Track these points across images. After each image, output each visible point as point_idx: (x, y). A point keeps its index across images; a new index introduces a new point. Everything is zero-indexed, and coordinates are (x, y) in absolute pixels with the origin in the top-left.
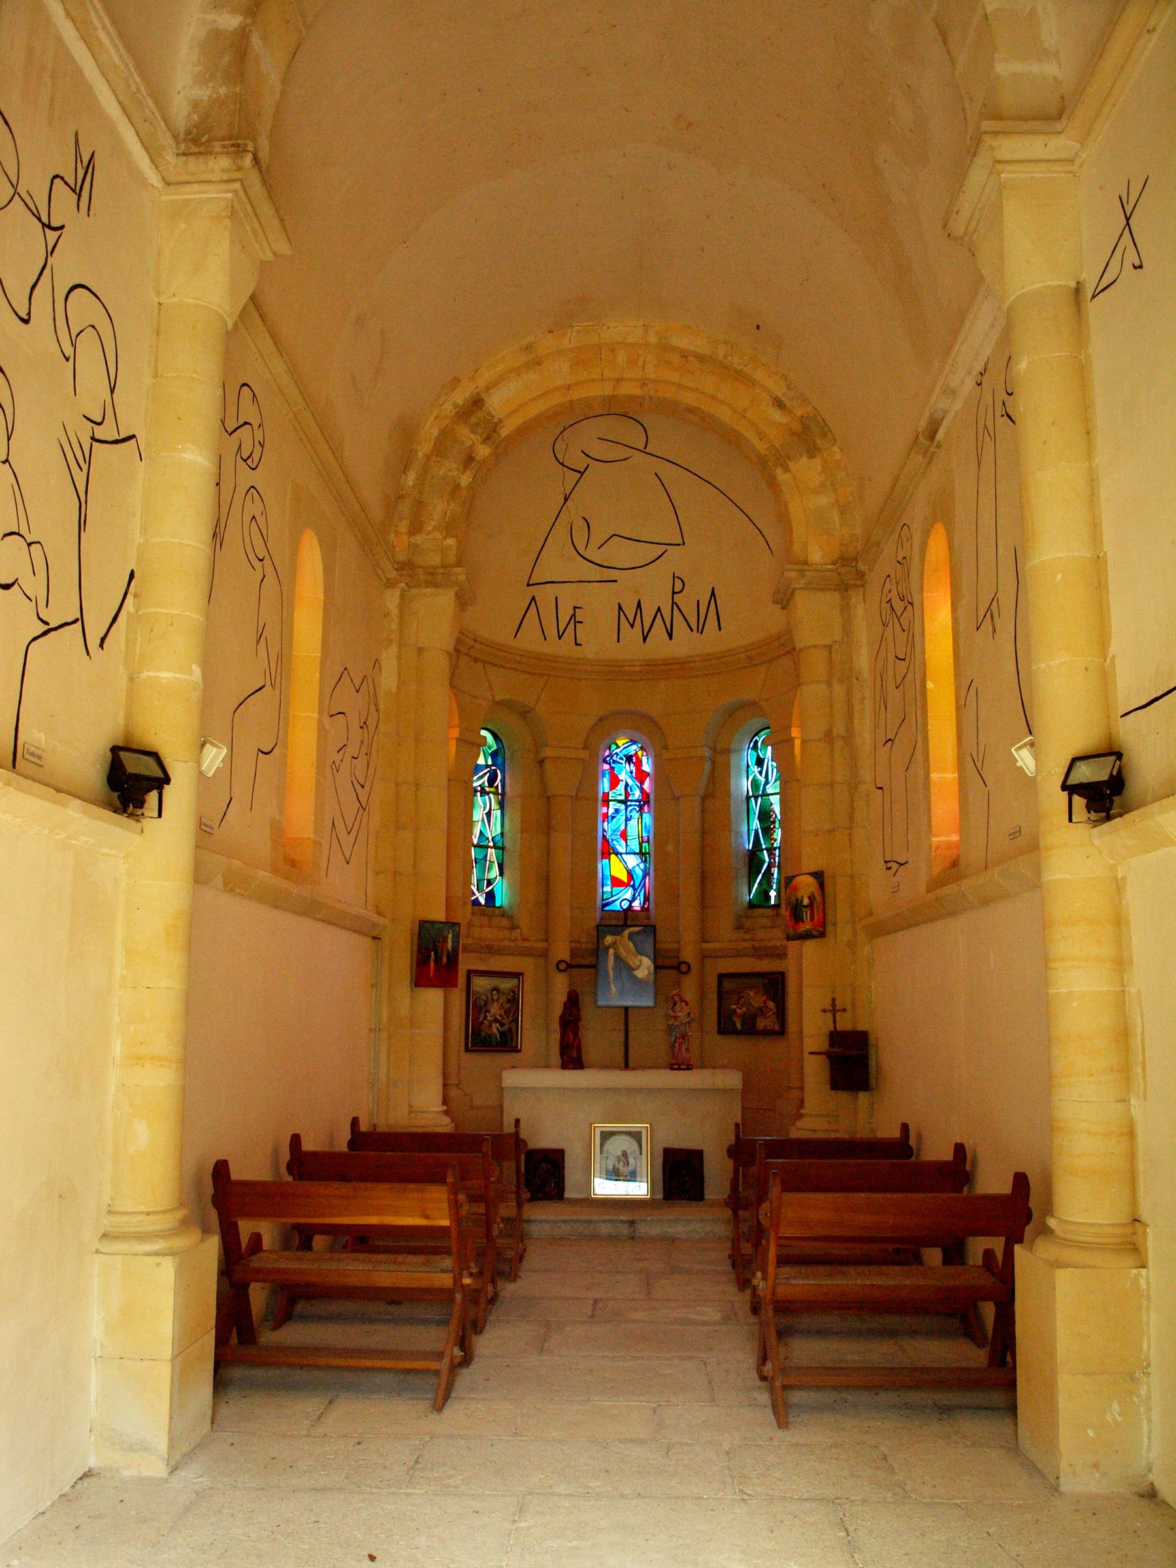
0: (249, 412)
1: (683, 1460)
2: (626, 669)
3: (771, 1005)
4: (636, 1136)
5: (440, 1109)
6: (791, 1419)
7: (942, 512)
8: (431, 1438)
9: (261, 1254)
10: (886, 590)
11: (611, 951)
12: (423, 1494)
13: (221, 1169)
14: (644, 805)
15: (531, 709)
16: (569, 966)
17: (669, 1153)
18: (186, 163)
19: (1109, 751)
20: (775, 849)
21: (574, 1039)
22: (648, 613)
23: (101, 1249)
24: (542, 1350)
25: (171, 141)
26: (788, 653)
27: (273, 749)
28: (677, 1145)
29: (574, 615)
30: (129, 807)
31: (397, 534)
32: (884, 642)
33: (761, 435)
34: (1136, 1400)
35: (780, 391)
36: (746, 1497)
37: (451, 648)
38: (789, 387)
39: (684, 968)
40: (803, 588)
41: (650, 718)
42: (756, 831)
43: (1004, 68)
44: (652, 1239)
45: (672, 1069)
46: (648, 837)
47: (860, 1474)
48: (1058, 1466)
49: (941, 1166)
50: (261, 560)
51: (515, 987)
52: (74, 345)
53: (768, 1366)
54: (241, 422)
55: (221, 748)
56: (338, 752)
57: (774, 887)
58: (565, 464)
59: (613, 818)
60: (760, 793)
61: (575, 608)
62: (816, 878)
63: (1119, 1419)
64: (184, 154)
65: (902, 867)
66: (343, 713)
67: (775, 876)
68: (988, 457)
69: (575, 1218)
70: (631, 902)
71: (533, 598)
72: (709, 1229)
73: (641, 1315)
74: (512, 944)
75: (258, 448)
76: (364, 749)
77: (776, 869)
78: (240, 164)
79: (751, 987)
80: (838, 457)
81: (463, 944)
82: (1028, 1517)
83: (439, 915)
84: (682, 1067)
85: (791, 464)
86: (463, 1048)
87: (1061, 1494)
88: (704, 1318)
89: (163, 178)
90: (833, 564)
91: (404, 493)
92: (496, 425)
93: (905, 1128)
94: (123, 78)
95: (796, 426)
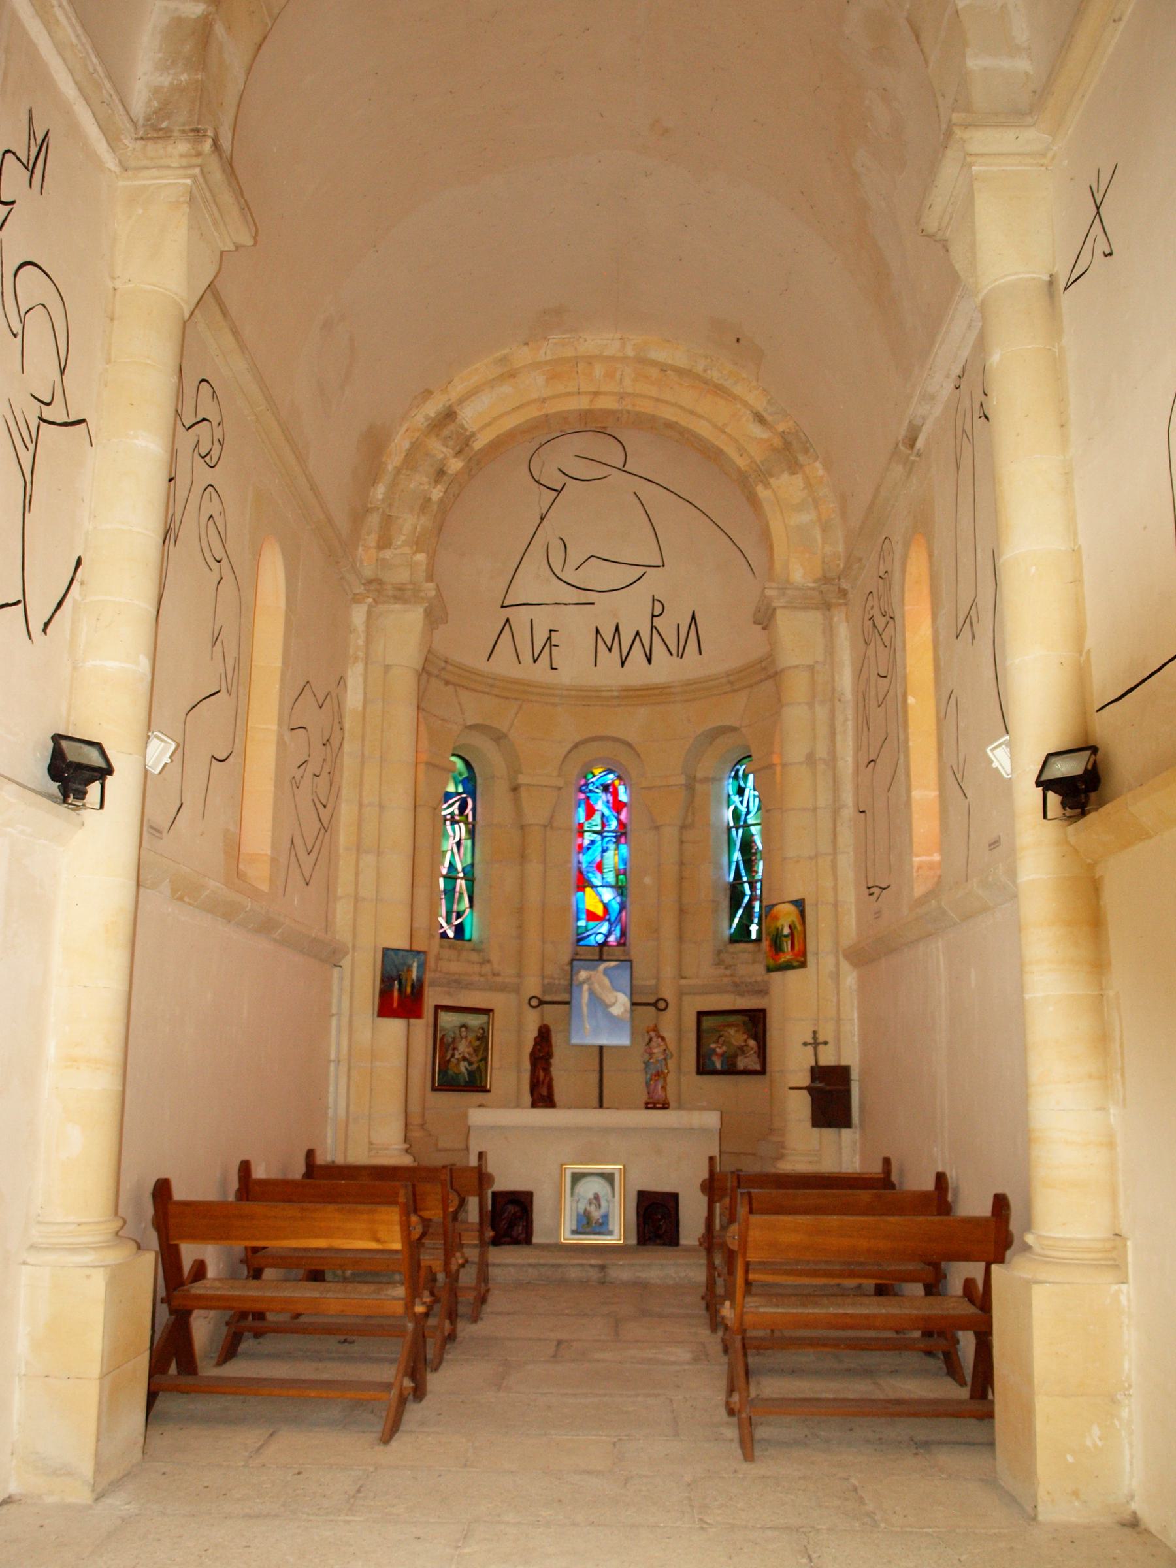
0: (207, 408)
1: (640, 1490)
2: (604, 694)
3: (752, 1043)
6: (756, 1453)
7: (922, 525)
8: (376, 1468)
10: (868, 608)
11: (586, 987)
16: (542, 1003)
17: (642, 1195)
20: (757, 881)
21: (545, 1076)
22: (627, 637)
23: (28, 1260)
24: (499, 1388)
25: (129, 125)
26: (769, 677)
27: (228, 757)
29: (549, 638)
32: (866, 660)
34: (1117, 1423)
35: (760, 405)
36: (705, 1526)
37: (419, 667)
39: (662, 1005)
41: (630, 746)
42: (737, 863)
43: (975, 63)
45: (647, 1108)
47: (827, 1504)
49: (924, 1195)
50: (219, 561)
52: (23, 323)
53: (736, 1398)
54: (200, 418)
56: (299, 767)
57: (756, 920)
59: (588, 849)
60: (742, 823)
62: (796, 906)
63: (1100, 1444)
64: (142, 138)
66: (305, 728)
68: (966, 462)
69: (542, 1261)
70: (607, 936)
71: (508, 620)
74: (482, 979)
75: (217, 446)
76: (327, 769)
78: (199, 149)
79: (730, 1025)
83: (399, 941)
84: (658, 1106)
85: (772, 480)
88: (673, 1358)
89: (120, 161)
90: (814, 582)
91: (373, 506)
93: (887, 1162)
94: (81, 58)
95: (777, 442)
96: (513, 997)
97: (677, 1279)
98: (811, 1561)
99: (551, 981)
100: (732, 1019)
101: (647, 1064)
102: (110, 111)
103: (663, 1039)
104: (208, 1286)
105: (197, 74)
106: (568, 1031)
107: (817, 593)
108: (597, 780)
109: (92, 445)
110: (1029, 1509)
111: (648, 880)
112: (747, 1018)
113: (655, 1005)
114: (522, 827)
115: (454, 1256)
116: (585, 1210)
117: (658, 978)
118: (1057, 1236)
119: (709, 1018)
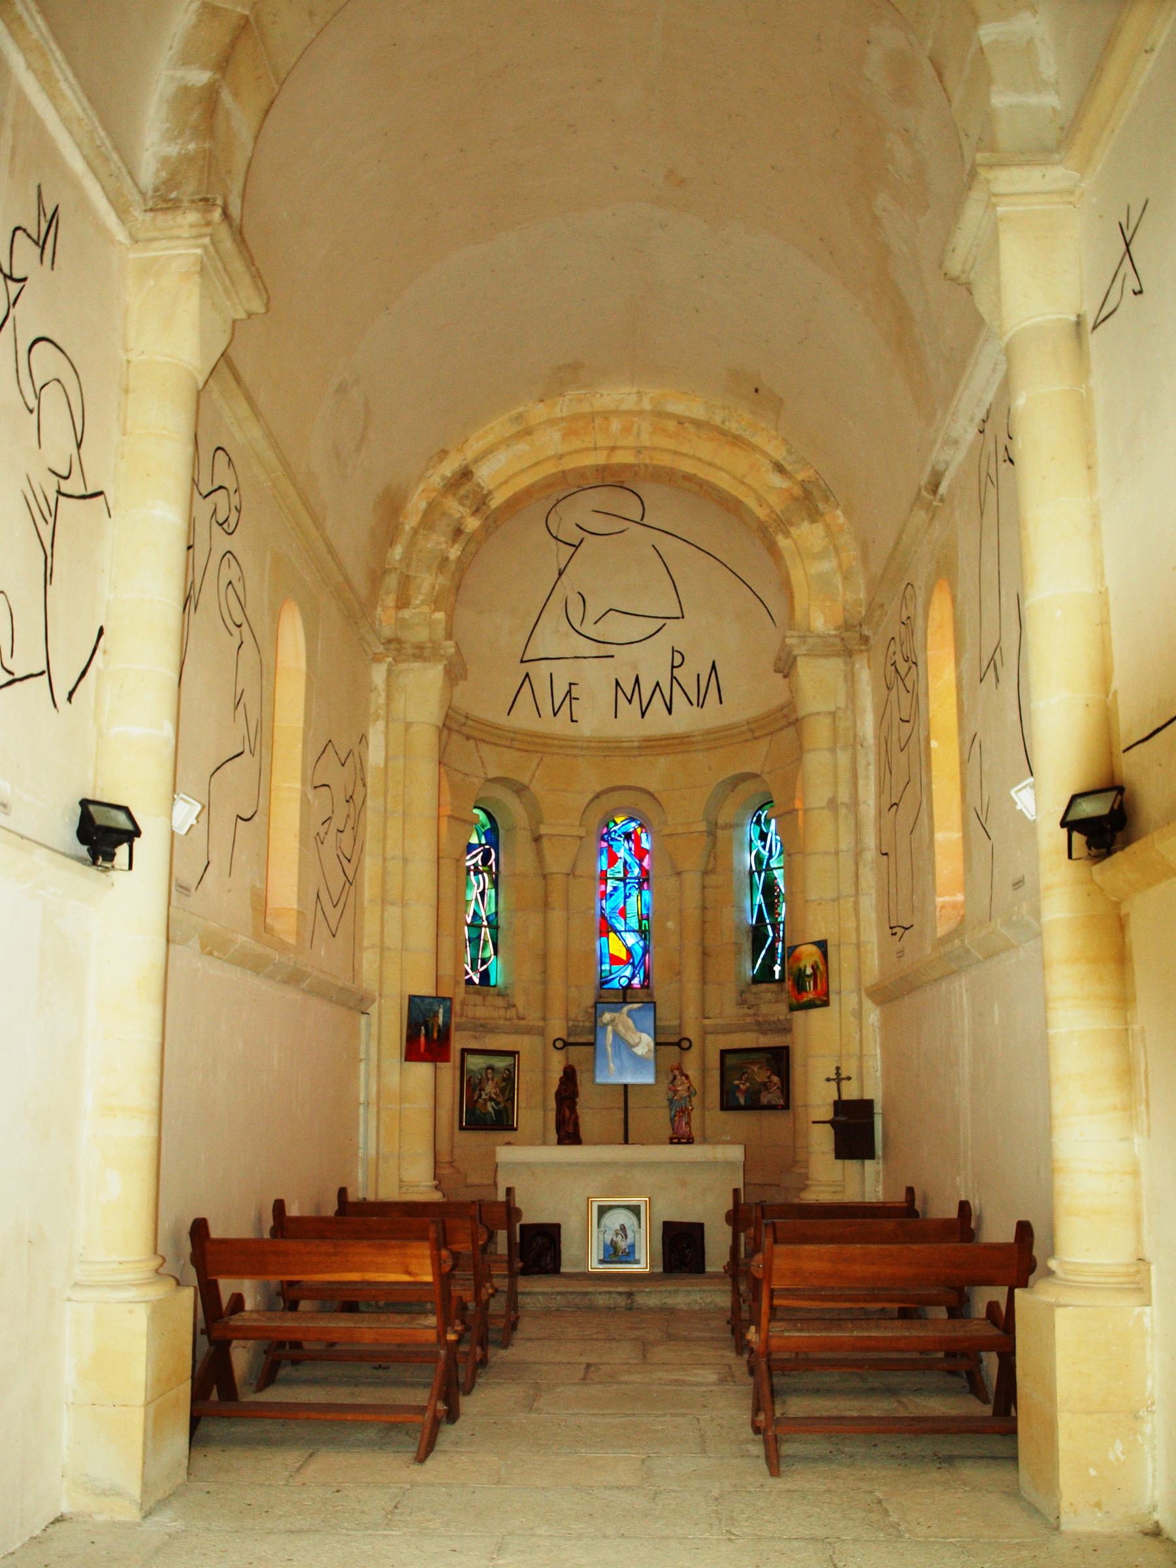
0: (224, 476)
2: (625, 744)
3: (775, 1079)
4: (635, 1210)
5: (430, 1184)
6: (783, 1468)
7: (945, 569)
8: (412, 1486)
9: (243, 1314)
11: (610, 1028)
12: (400, 1535)
13: (199, 1228)
14: (643, 882)
15: (525, 786)
16: (566, 1044)
17: (668, 1226)
18: (153, 220)
19: (1110, 786)
21: (571, 1114)
22: (646, 689)
25: (138, 197)
26: (790, 724)
27: (253, 816)
28: (677, 1218)
29: (569, 692)
30: (98, 859)
31: (385, 608)
33: (761, 501)
35: (779, 454)
36: (733, 1537)
38: (789, 452)
39: (685, 1044)
40: (805, 655)
42: (760, 906)
44: (651, 1310)
45: (672, 1143)
46: (648, 914)
48: (1059, 1506)
49: (946, 1224)
50: (239, 626)
51: (510, 1065)
52: (38, 398)
53: (761, 1417)
54: (216, 486)
55: (192, 804)
56: (323, 824)
57: (779, 961)
58: (559, 537)
59: (611, 895)
60: (764, 867)
61: (570, 684)
62: (819, 947)
63: (1122, 1458)
64: (151, 210)
65: (907, 931)
66: (328, 786)
67: (780, 951)
69: (570, 1289)
70: (630, 980)
71: (527, 675)
72: (710, 1300)
73: (635, 1377)
74: (507, 1023)
75: (234, 514)
76: (350, 824)
77: (780, 943)
79: (753, 1063)
80: (841, 520)
81: (456, 1022)
82: (1025, 1553)
83: (425, 988)
84: (683, 1141)
85: (792, 530)
86: (457, 1125)
87: (1061, 1533)
88: (699, 1379)
89: (130, 234)
92: (487, 496)
93: (910, 1191)
95: (797, 491)
96: (538, 1040)
97: (703, 1305)
99: (575, 1023)
100: (755, 1056)
101: (671, 1101)
103: (687, 1077)
104: (246, 1317)
106: (593, 1071)
108: (619, 829)
110: (1052, 1520)
111: (670, 924)
112: (770, 1056)
113: (678, 1044)
114: (545, 876)
115: (484, 1286)
116: (612, 1240)
117: (681, 1018)
119: (732, 1056)
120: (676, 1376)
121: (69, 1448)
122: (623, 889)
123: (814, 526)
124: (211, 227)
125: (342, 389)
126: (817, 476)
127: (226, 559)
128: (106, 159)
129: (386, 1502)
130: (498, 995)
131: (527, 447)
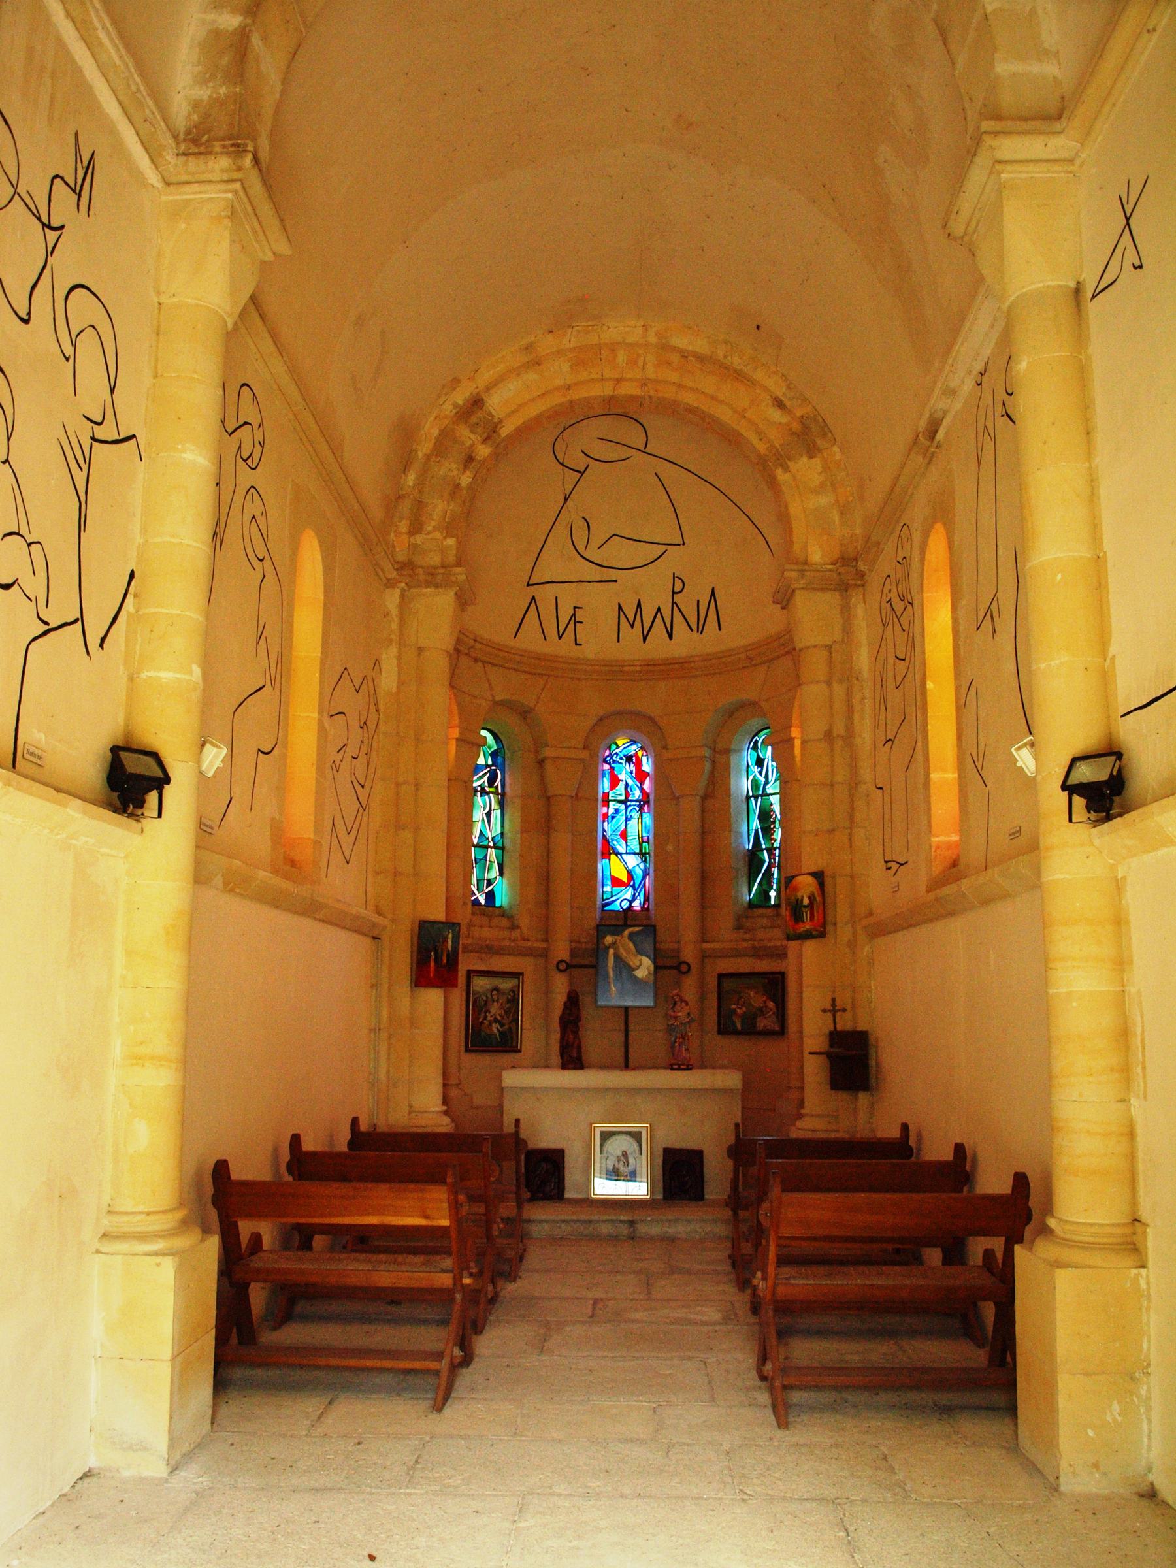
0: (249, 412)
2: (626, 669)
3: (771, 1004)
4: (636, 1136)
6: (791, 1419)
7: (942, 511)
8: (431, 1438)
9: (261, 1254)
10: (886, 590)
11: (611, 951)
12: (422, 1494)
17: (669, 1153)
18: (186, 163)
19: (1109, 751)
20: (775, 849)
24: (542, 1351)
25: (171, 141)
26: (788, 653)
27: (273, 749)
28: (677, 1146)
29: (574, 615)
30: (129, 807)
31: (397, 534)
32: (884, 642)
33: (761, 436)
34: (1136, 1399)
35: (780, 391)
36: (746, 1497)
37: (451, 649)
39: (684, 968)
40: (803, 588)
41: (651, 718)
42: (756, 831)
43: (1004, 68)
45: (672, 1069)
46: (648, 837)
47: (860, 1474)
48: (1058, 1466)
49: (941, 1166)
50: (261, 560)
51: (515, 987)
52: (74, 346)
53: (768, 1367)
56: (338, 752)
57: (774, 887)
58: (565, 464)
59: (613, 818)
60: (760, 793)
61: (575, 608)
63: (1119, 1419)
64: (184, 154)
67: (775, 876)
68: (988, 458)
70: (631, 902)
71: (533, 598)
72: (709, 1229)
74: (512, 944)
75: (258, 448)
76: (364, 749)
77: (776, 869)
78: (240, 164)
80: (838, 457)
83: (439, 915)
84: (682, 1067)
85: (791, 464)
86: (463, 1048)
87: (1061, 1494)
88: (704, 1318)
89: (163, 178)
91: (404, 493)
92: (496, 425)
93: (905, 1127)
95: (796, 426)
98: (848, 1535)
102: (153, 129)
105: (236, 88)
107: (835, 575)
109: (141, 460)
110: (1052, 1480)
118: (1078, 1220)
120: (681, 1313)
121: (96, 1403)
122: (624, 811)
123: (814, 460)
124: (241, 172)
125: (360, 321)
126: (816, 413)
127: (250, 492)
128: (140, 105)
129: (407, 1456)
130: (503, 916)
131: (536, 376)
